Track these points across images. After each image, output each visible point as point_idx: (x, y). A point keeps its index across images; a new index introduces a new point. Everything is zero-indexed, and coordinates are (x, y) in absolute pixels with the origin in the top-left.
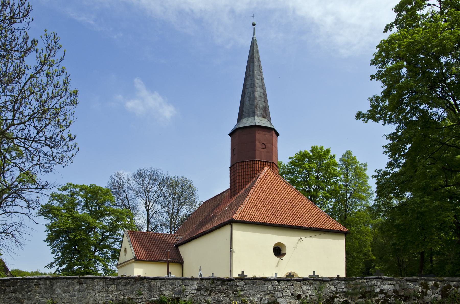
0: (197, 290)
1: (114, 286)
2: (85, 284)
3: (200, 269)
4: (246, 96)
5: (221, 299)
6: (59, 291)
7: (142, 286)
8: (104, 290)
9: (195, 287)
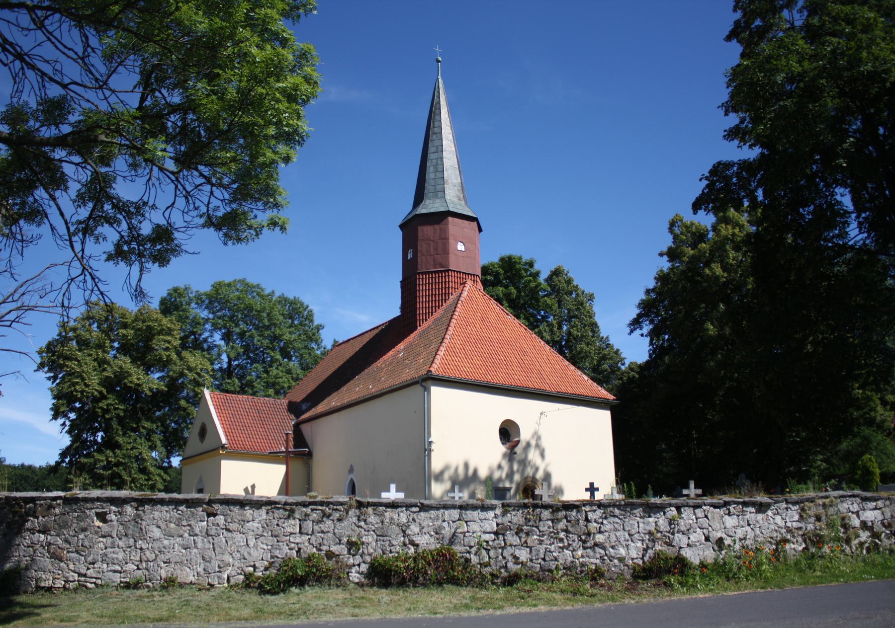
0: (496, 533)
1: (293, 522)
2: (222, 517)
3: (351, 470)
4: (428, 164)
5: (554, 554)
6: (156, 533)
7: (362, 524)
8: (267, 533)
9: (491, 525)
